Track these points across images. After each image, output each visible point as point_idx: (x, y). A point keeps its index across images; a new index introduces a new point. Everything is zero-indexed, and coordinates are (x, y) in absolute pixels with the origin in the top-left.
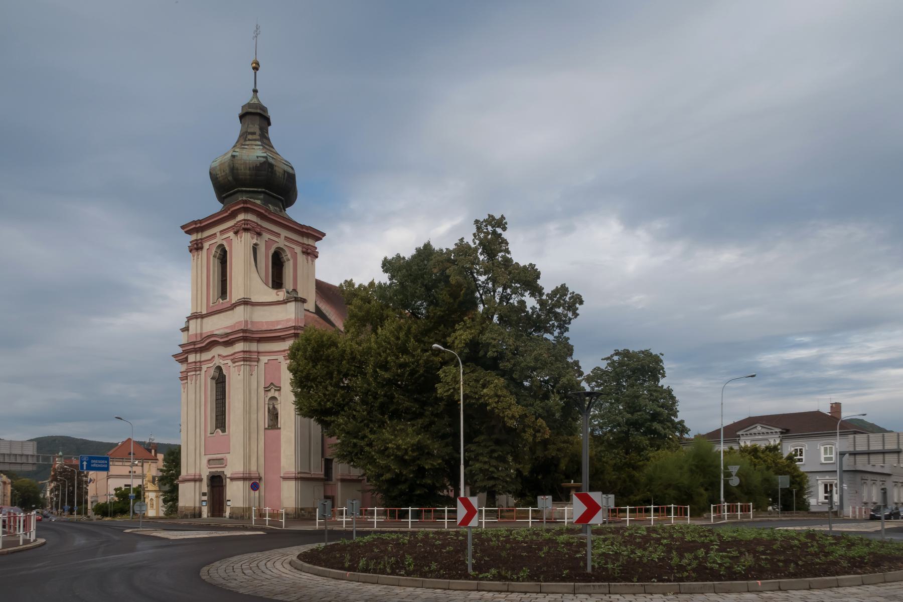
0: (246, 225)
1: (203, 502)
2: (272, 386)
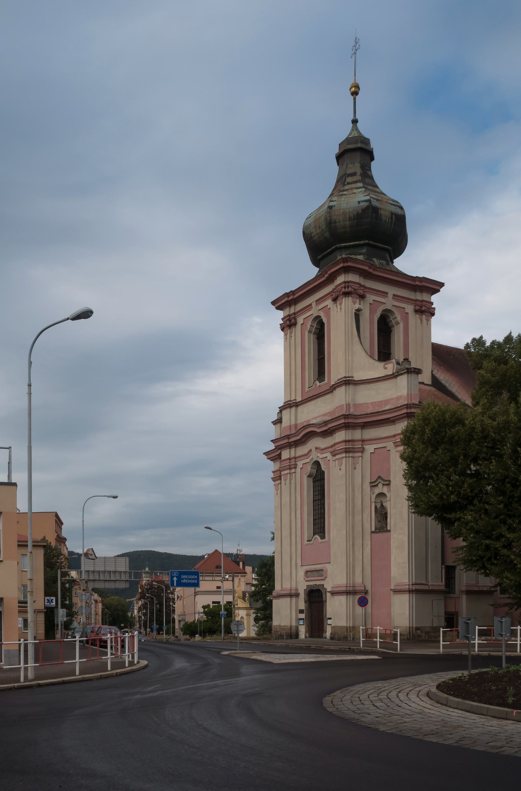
0: (347, 289)
2: (380, 480)
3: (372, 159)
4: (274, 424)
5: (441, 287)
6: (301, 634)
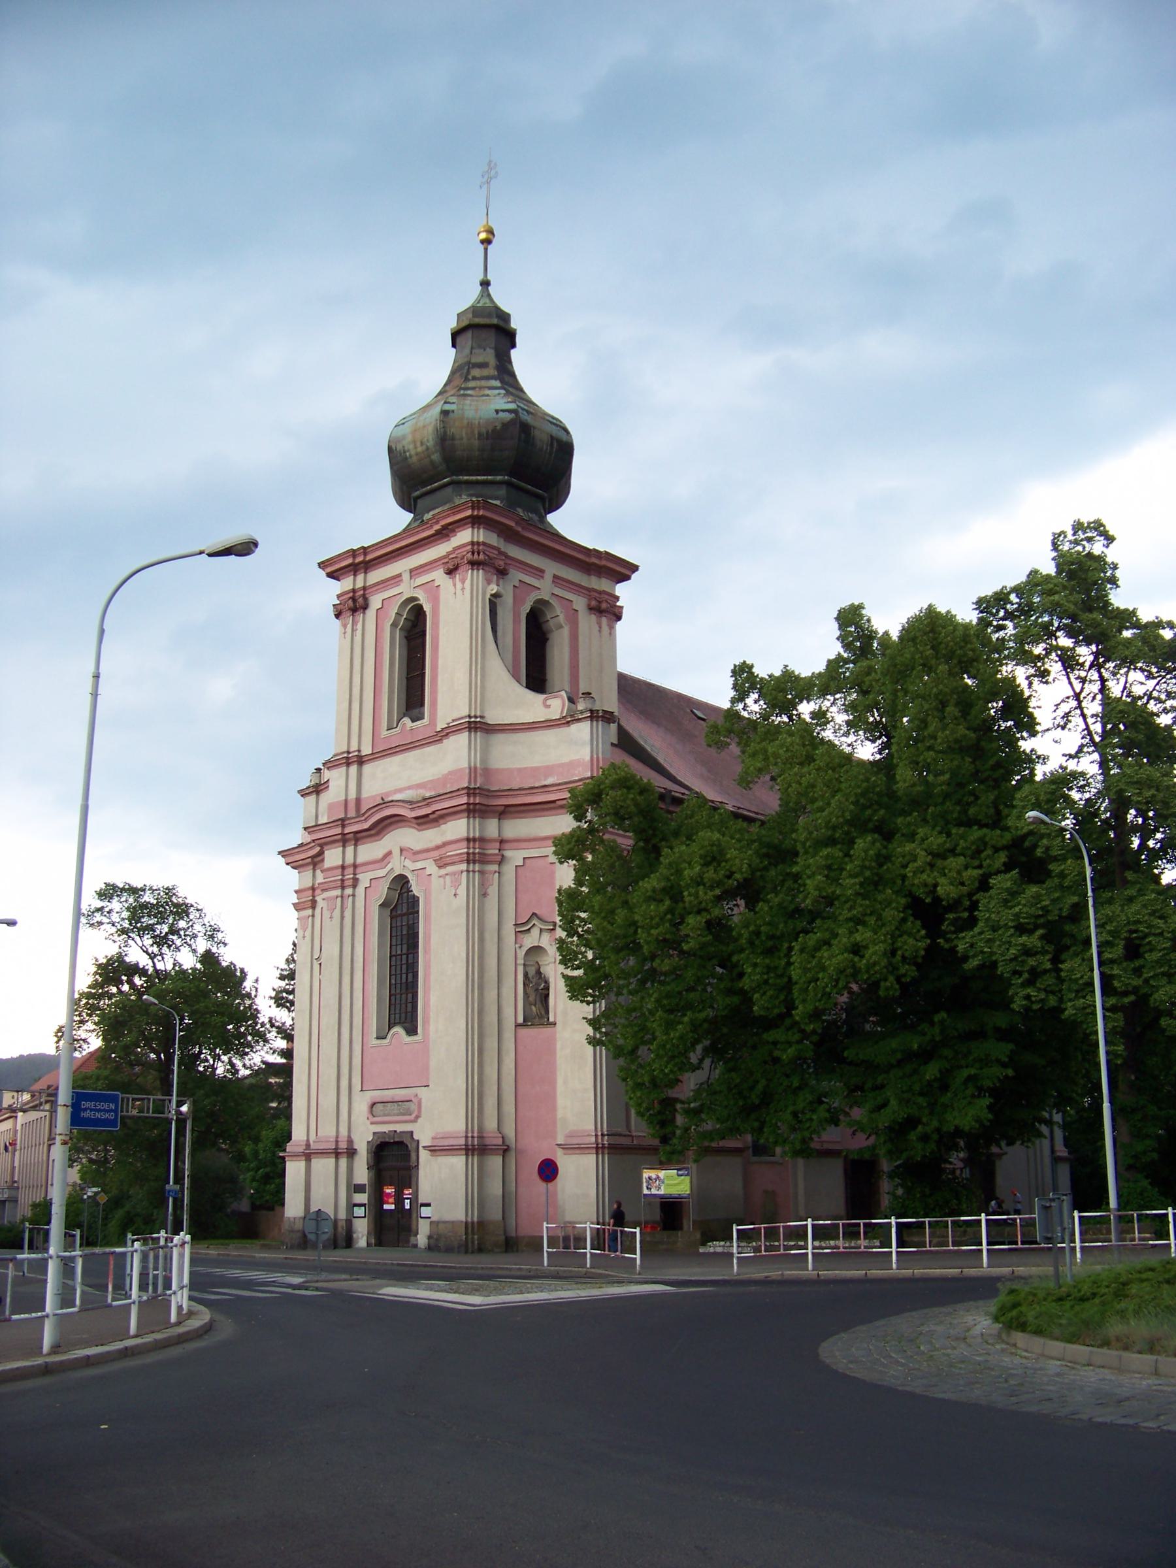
1: (356, 1209)
2: (535, 921)
3: (513, 346)
4: (302, 796)
5: (634, 572)
6: (358, 1238)
